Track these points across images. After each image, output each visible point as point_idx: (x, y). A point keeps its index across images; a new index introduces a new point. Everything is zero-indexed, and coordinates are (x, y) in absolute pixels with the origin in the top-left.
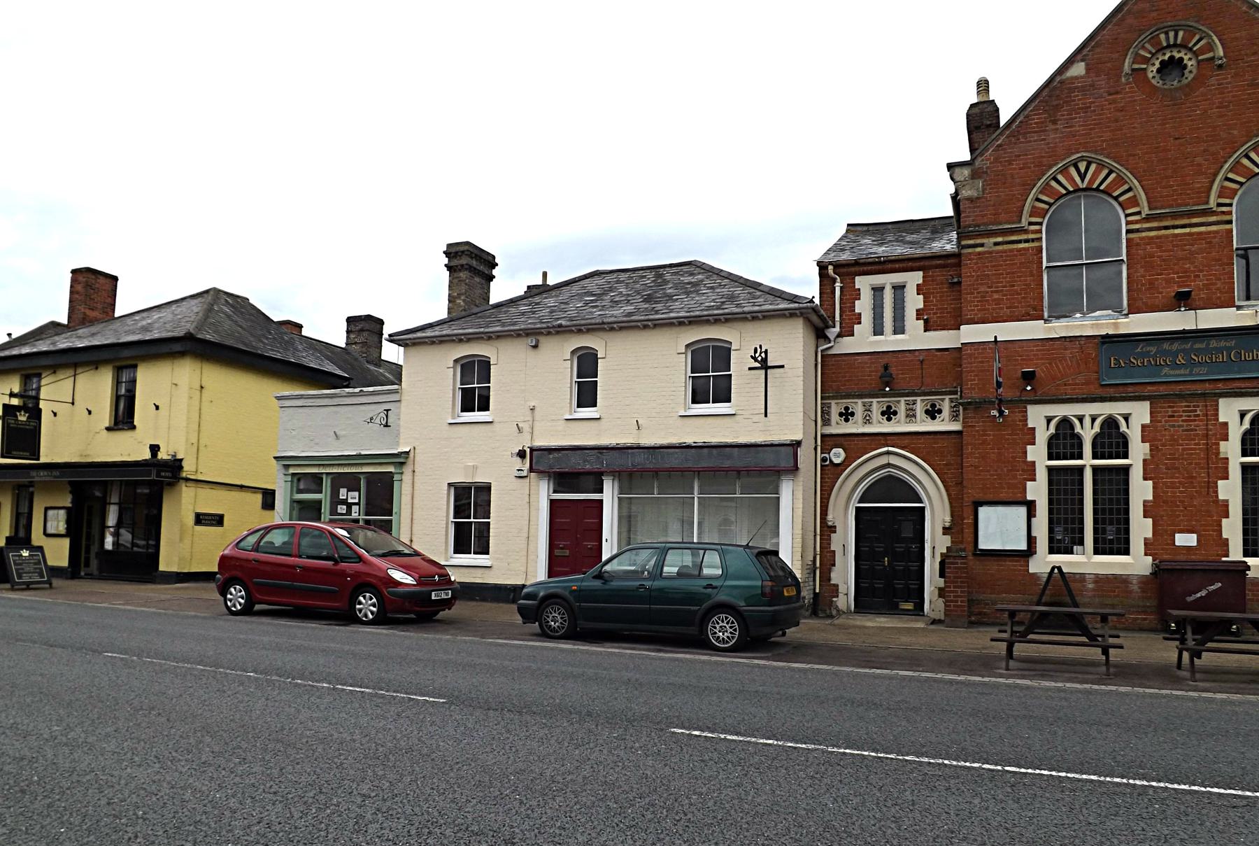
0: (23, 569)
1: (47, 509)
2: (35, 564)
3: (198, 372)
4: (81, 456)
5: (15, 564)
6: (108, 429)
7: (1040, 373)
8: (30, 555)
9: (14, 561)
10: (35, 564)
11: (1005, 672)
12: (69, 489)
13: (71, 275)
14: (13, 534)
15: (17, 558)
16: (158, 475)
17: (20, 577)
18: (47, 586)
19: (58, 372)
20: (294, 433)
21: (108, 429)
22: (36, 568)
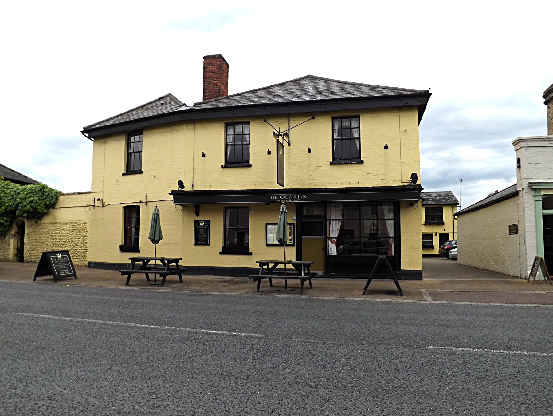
0: (59, 267)
1: (267, 224)
2: (66, 263)
3: (104, 145)
4: (303, 184)
5: (55, 264)
6: (123, 175)
7: (118, 180)
8: (62, 257)
9: (54, 262)
10: (66, 263)
11: (124, 288)
12: (195, 210)
13: (203, 60)
14: (123, 244)
15: (55, 260)
16: (286, 201)
17: (59, 273)
18: (74, 277)
19: (316, 119)
20: (539, 166)
21: (331, 164)
22: (66, 266)
